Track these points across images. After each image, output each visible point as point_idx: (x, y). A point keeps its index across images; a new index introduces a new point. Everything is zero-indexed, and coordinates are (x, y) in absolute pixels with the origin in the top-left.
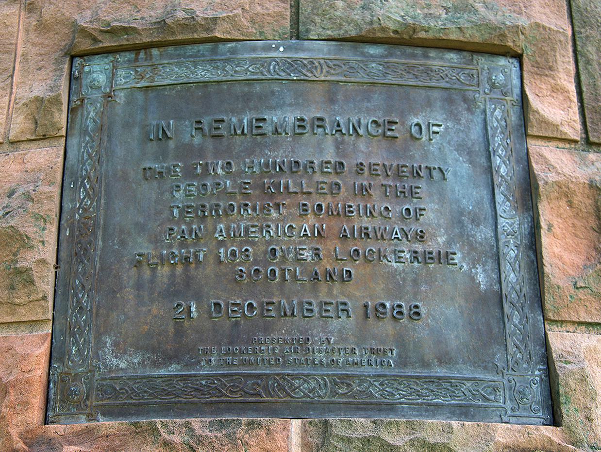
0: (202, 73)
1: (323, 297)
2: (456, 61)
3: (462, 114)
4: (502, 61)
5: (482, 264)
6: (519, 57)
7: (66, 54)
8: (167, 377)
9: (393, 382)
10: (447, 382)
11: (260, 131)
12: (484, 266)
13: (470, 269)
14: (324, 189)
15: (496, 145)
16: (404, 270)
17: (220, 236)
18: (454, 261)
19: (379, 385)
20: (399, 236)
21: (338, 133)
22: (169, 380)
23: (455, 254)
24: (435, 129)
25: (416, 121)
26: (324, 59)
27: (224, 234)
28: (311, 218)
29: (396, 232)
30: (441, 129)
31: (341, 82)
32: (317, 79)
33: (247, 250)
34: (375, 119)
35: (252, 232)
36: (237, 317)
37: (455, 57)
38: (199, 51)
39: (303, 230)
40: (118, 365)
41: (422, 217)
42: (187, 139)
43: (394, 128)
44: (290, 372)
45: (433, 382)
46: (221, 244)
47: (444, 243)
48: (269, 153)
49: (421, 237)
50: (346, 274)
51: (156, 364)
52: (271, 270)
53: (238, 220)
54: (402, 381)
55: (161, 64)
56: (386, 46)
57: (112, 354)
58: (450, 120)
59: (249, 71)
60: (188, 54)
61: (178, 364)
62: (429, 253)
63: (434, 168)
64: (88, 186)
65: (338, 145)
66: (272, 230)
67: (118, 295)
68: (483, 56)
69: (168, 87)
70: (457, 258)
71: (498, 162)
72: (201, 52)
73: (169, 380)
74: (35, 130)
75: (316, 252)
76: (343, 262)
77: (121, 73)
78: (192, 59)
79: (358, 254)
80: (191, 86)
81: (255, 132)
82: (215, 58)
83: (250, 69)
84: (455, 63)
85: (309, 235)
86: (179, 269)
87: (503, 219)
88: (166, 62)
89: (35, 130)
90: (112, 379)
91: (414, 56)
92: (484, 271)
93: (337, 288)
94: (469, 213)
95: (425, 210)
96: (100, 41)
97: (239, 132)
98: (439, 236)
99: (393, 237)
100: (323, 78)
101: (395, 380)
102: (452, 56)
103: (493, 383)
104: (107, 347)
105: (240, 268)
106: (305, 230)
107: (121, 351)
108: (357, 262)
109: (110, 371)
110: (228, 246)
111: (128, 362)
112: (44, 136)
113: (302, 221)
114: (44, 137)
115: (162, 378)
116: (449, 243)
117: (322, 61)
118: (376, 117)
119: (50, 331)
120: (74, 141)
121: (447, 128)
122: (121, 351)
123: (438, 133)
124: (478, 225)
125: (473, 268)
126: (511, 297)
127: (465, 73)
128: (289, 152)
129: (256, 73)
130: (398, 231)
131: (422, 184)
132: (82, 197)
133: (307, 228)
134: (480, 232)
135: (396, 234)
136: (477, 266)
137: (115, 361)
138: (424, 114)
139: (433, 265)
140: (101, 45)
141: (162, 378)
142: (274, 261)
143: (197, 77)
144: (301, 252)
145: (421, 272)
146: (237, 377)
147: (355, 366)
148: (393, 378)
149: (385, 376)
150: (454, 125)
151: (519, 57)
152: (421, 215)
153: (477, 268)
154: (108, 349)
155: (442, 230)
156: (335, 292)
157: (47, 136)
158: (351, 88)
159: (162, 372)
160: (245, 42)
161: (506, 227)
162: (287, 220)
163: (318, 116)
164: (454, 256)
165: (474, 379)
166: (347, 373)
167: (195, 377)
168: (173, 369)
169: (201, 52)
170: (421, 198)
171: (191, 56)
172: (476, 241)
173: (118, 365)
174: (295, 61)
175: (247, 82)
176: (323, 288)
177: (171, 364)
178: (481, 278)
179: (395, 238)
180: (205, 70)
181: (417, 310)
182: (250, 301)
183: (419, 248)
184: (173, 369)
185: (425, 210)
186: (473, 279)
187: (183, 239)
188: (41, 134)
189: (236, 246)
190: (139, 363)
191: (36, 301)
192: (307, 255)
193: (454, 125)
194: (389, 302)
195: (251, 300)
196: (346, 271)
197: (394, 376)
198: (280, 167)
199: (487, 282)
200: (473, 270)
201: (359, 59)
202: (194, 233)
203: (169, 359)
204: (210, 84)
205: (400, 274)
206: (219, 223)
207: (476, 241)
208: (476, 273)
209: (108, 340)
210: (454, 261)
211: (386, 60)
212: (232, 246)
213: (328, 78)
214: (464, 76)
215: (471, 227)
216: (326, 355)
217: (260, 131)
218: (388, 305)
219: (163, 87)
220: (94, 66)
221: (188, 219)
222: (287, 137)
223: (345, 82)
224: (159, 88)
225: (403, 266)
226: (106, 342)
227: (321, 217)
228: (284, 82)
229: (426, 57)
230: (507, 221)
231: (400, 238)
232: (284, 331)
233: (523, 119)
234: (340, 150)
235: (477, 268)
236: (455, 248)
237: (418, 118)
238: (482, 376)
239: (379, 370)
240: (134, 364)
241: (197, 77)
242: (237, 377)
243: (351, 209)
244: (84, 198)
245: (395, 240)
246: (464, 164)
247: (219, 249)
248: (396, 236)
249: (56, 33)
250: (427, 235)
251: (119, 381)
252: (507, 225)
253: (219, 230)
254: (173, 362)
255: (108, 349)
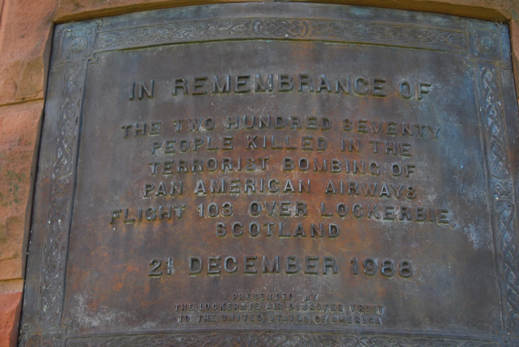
0: (185, 34)
1: (307, 251)
2: (444, 24)
3: (451, 76)
4: (490, 26)
5: (475, 223)
6: (507, 22)
7: (48, 21)
8: (142, 334)
9: (382, 339)
10: (439, 341)
11: (242, 88)
12: (477, 225)
13: (463, 228)
14: (309, 144)
15: (487, 106)
16: (392, 227)
17: (199, 191)
18: (446, 219)
19: (367, 343)
20: (387, 192)
21: (323, 90)
22: (144, 337)
23: (446, 212)
24: (424, 88)
25: (403, 80)
26: (309, 19)
27: (204, 189)
28: (295, 173)
29: (384, 188)
30: (430, 89)
31: (327, 41)
32: (302, 38)
33: (227, 205)
34: (361, 77)
35: (233, 187)
36: (215, 273)
37: (443, 21)
38: (181, 13)
39: (286, 185)
40: (90, 324)
41: (411, 174)
42: (168, 97)
43: (381, 86)
44: (271, 328)
45: (424, 340)
46: (200, 200)
47: (434, 201)
48: (252, 110)
49: (412, 194)
50: (332, 230)
51: (130, 322)
52: (252, 226)
53: (219, 176)
54: (391, 339)
55: (143, 27)
56: (372, 9)
57: (85, 312)
58: (439, 81)
59: (233, 31)
60: (170, 17)
61: (153, 321)
62: (419, 210)
63: (423, 127)
64: (66, 146)
65: (323, 103)
66: (254, 185)
67: (92, 253)
68: (471, 21)
69: (149, 49)
70: (449, 215)
71: (490, 123)
72: (184, 15)
73: (144, 337)
74: (15, 94)
75: (300, 207)
76: (328, 218)
77: (103, 37)
78: (175, 21)
79: (344, 210)
80: (173, 47)
81: (237, 89)
82: (197, 19)
83: (234, 28)
84: (444, 26)
85: (293, 190)
86: (157, 225)
87: (496, 179)
88: (147, 24)
89: (15, 94)
90: (84, 337)
91: (400, 19)
92: (476, 230)
93: (322, 243)
94: (461, 172)
95: (413, 167)
96: (83, 7)
97: (221, 89)
98: (429, 194)
99: (381, 193)
100: (307, 37)
101: (384, 337)
102: (438, 19)
103: (487, 343)
104: (79, 306)
105: (220, 224)
106: (288, 186)
107: (94, 309)
108: (343, 218)
109: (82, 330)
110: (208, 201)
111: (101, 320)
112: (23, 99)
113: (286, 177)
114: (23, 101)
115: (135, 335)
116: (440, 201)
117: (307, 22)
118: (362, 76)
119: (21, 291)
120: (53, 105)
121: (436, 88)
122: (94, 309)
123: (426, 92)
124: (470, 184)
125: (466, 226)
126: (505, 256)
127: (453, 36)
128: (273, 108)
129: (240, 32)
130: (386, 187)
131: (411, 141)
132: (59, 157)
133: (290, 183)
134: (472, 191)
135: (384, 190)
136: (470, 225)
137: (87, 319)
138: (412, 74)
139: (423, 222)
140: (83, 10)
141: (135, 335)
142: (256, 217)
143: (180, 37)
144: (284, 207)
145: (411, 229)
146: (215, 333)
147: (342, 323)
148: (381, 336)
149: (372, 333)
150: (443, 86)
151: (507, 22)
152: (409, 172)
153: (469, 227)
154: (81, 307)
155: (432, 187)
156: (320, 248)
157: (26, 100)
158: (337, 47)
159: (136, 329)
160: (229, 4)
161: (499, 186)
162: (270, 175)
163: (303, 73)
164: (445, 214)
165: (467, 338)
166: (333, 330)
167: (171, 333)
168: (149, 325)
169: (184, 15)
170: (409, 156)
171: (173, 18)
172: (468, 200)
173: (90, 324)
174: (281, 20)
175: (230, 42)
176: (308, 242)
177: (146, 321)
178: (473, 237)
179: (383, 194)
180: (187, 31)
181: (406, 267)
182: (230, 257)
183: (408, 203)
184: (149, 325)
185: (413, 167)
186: (465, 238)
187: (161, 195)
188: (21, 98)
189: (216, 202)
190: (112, 321)
191: (8, 259)
192: (293, 210)
193: (443, 86)
194: (378, 259)
195: (231, 256)
196: (332, 227)
197: (382, 333)
198: (262, 123)
199: (480, 241)
200: (465, 229)
201: (345, 20)
202: (172, 189)
203: (143, 317)
204: (192, 44)
205: (388, 231)
206: (199, 179)
207: (468, 200)
208: (469, 232)
209: (81, 299)
210: (446, 219)
211: (372, 22)
212: (212, 201)
213: (314, 38)
214: (452, 39)
215: (462, 186)
216: (310, 311)
217: (242, 88)
218: (376, 261)
219: (145, 49)
220: (76, 32)
221: (166, 175)
222: (271, 95)
223: (330, 42)
224: (140, 50)
225: (392, 223)
226: (79, 300)
227: (305, 172)
228: (268, 41)
229: (413, 19)
230: (500, 180)
231: (388, 194)
232: (265, 288)
233: (513, 82)
234: (325, 108)
235: (469, 227)
236: (447, 206)
237: (405, 78)
238: (476, 336)
239: (367, 327)
240: (107, 322)
241: (180, 37)
242: (215, 333)
243: (337, 165)
244: (61, 158)
245: (384, 197)
246: (454, 124)
247: (198, 205)
248: (384, 192)
249: (41, 3)
250: (416, 192)
251: (91, 339)
252: (500, 184)
253: (198, 185)
254: (147, 319)
255: (81, 307)
